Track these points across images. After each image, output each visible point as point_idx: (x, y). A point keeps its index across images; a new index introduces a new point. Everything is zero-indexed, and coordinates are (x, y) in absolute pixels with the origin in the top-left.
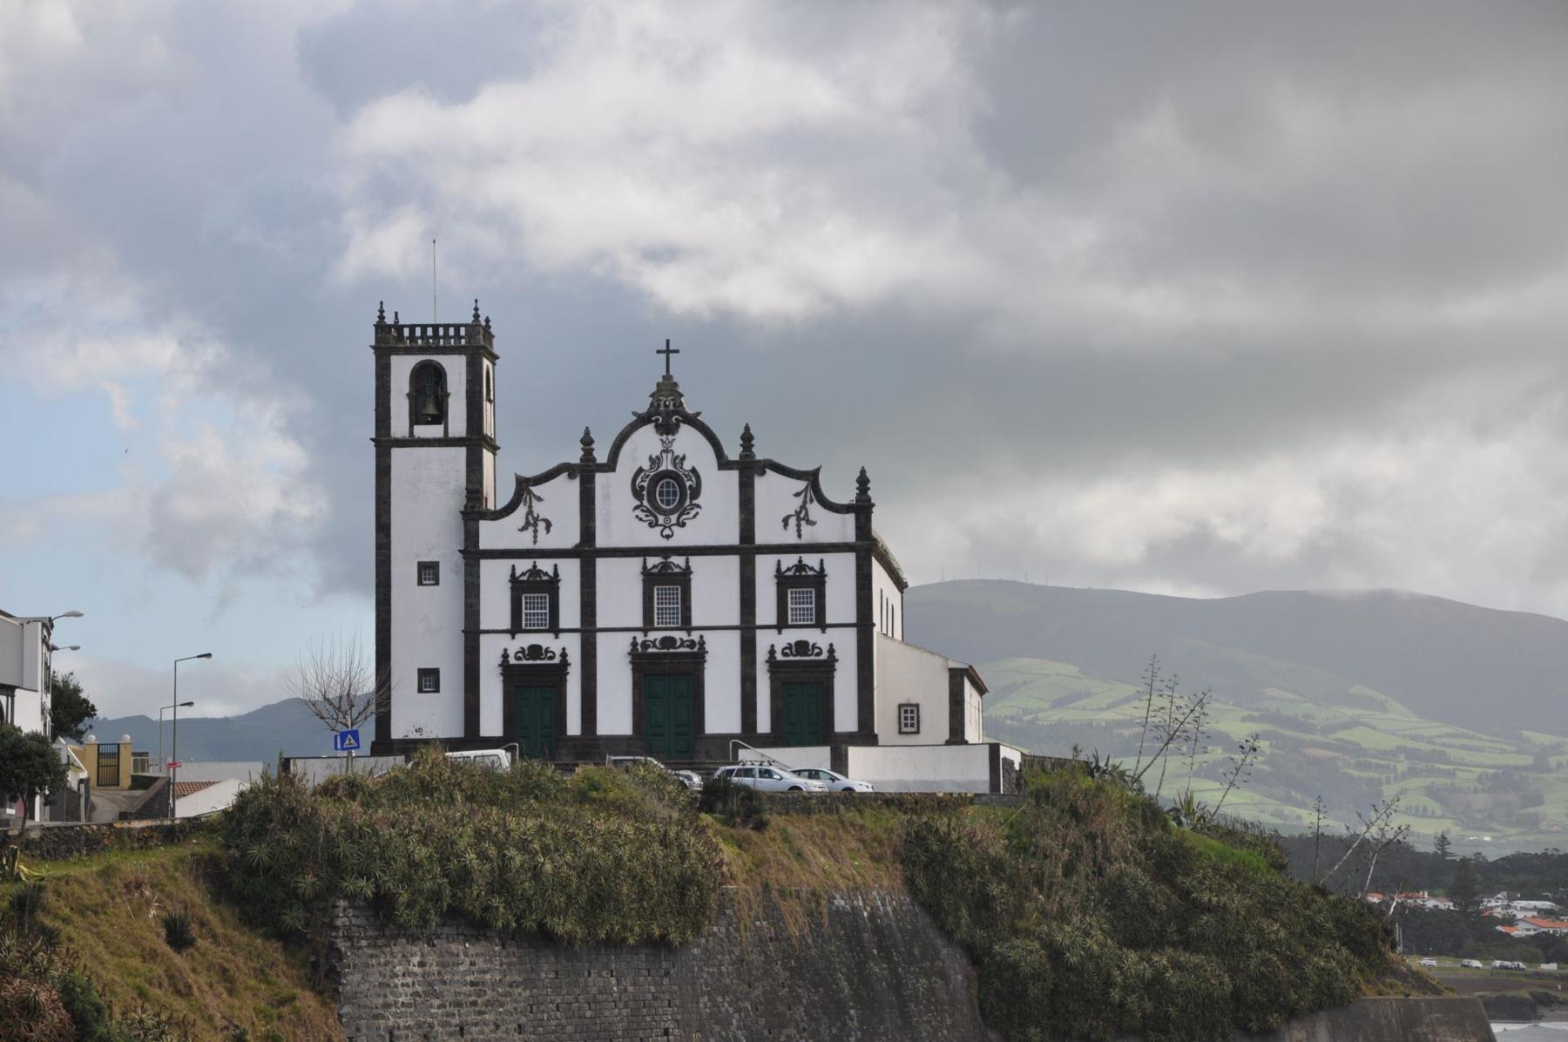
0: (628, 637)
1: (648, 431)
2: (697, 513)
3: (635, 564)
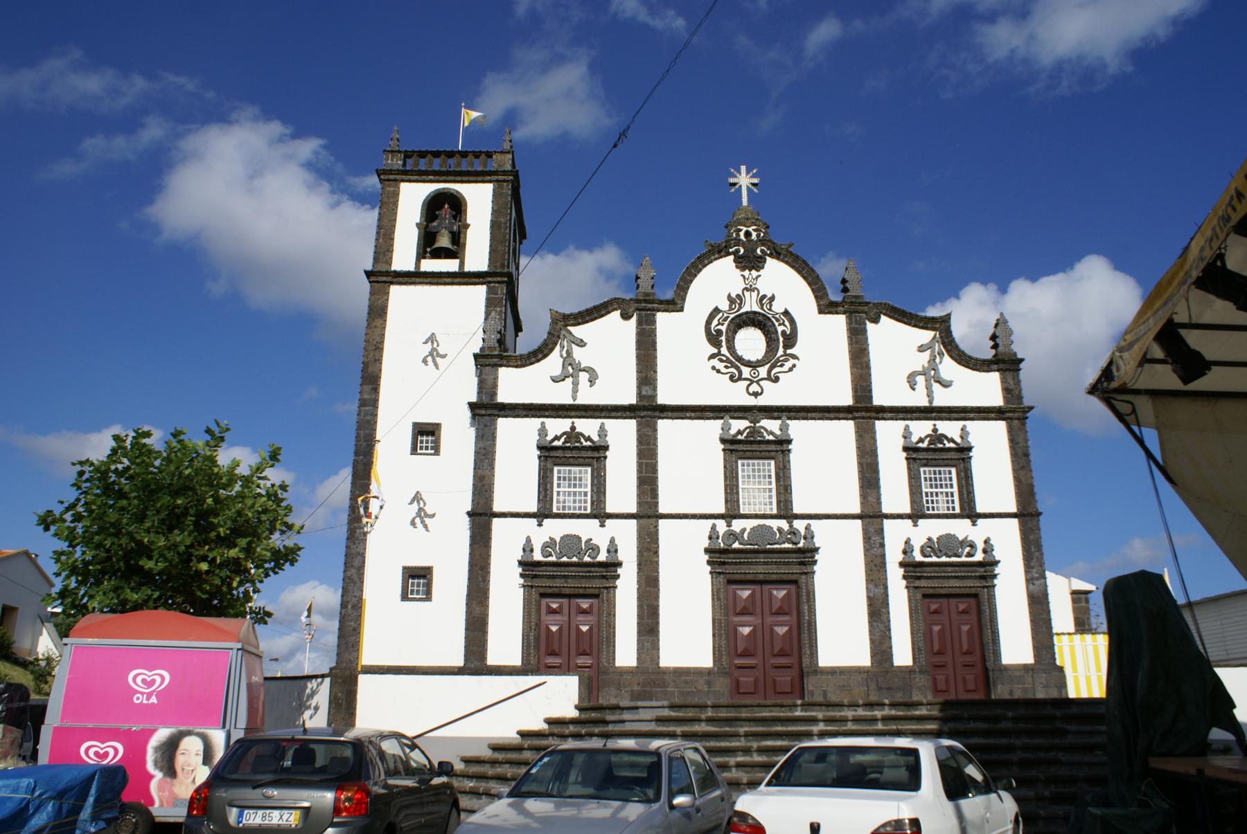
2: (794, 366)
3: (713, 428)
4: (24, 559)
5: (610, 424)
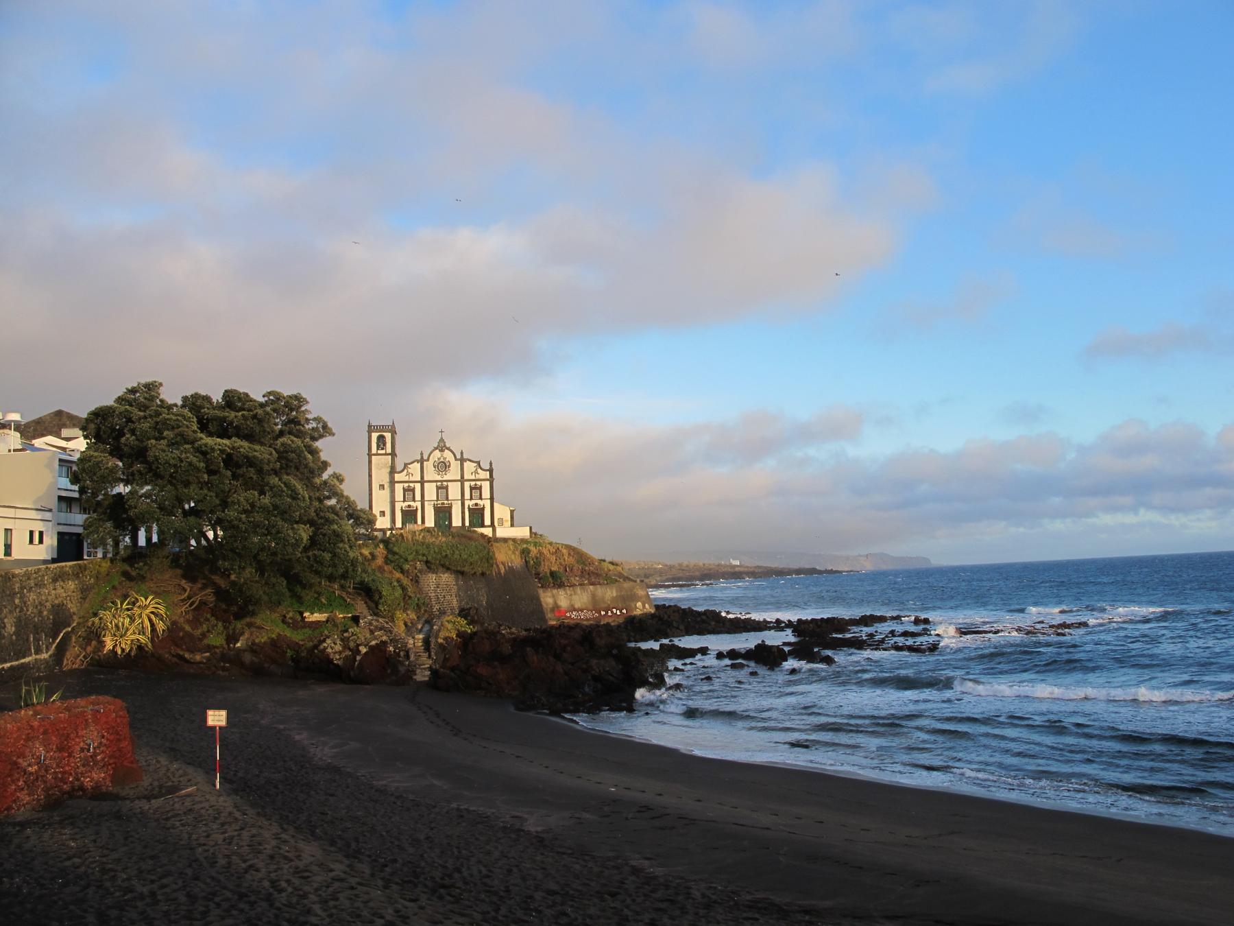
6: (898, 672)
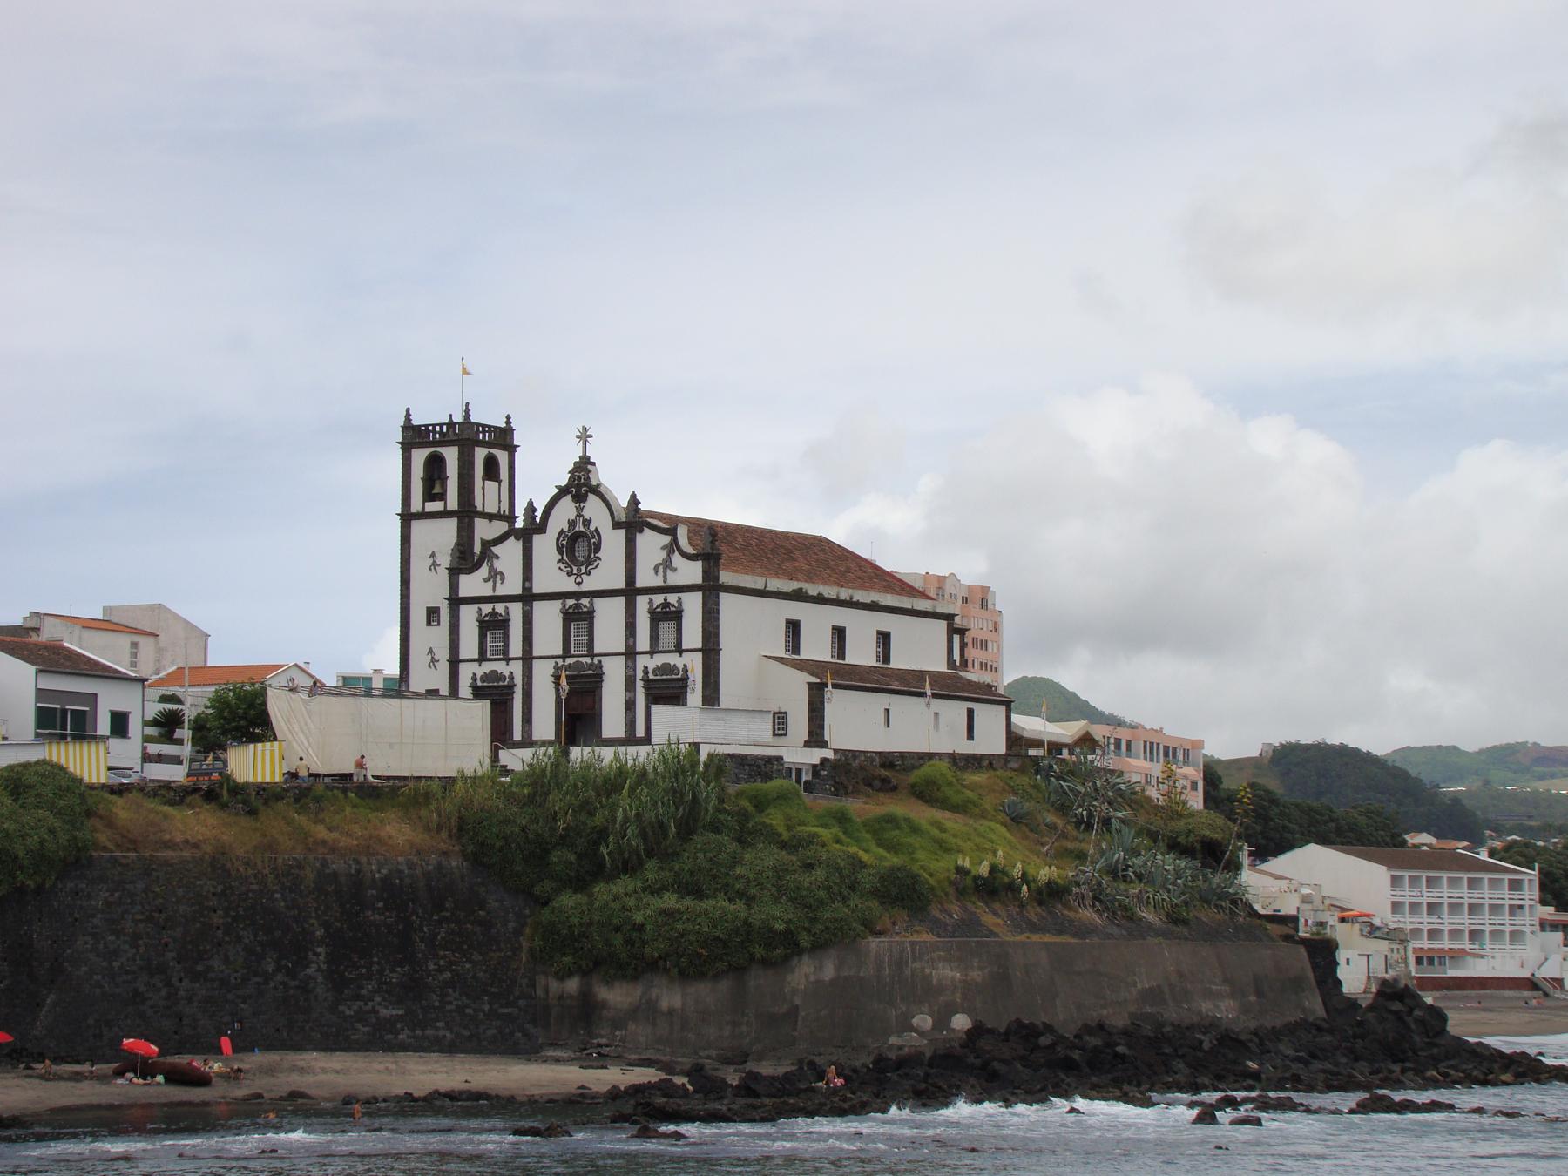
0: (552, 662)
1: (567, 501)
2: (598, 564)
3: (557, 605)
4: (295, 669)
5: (510, 605)
6: (391, 1136)
